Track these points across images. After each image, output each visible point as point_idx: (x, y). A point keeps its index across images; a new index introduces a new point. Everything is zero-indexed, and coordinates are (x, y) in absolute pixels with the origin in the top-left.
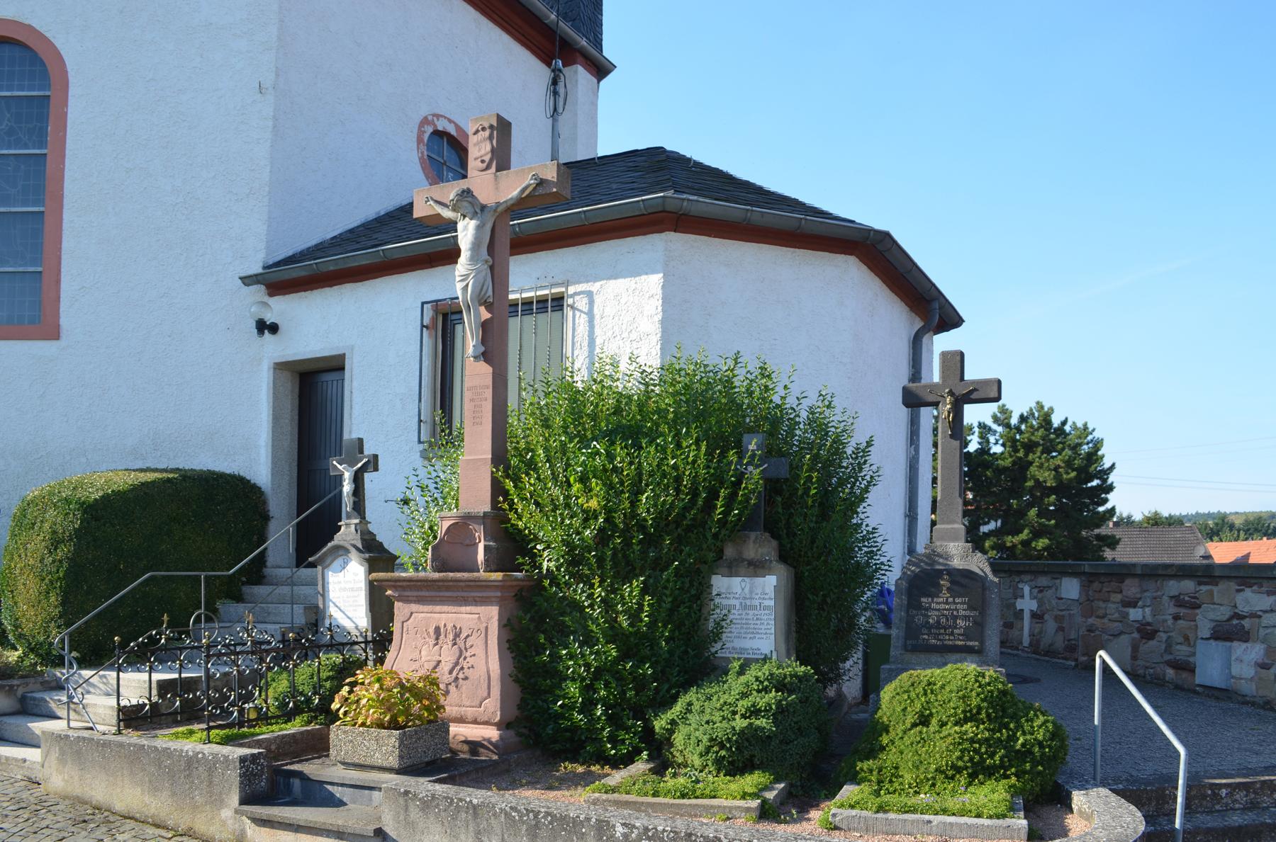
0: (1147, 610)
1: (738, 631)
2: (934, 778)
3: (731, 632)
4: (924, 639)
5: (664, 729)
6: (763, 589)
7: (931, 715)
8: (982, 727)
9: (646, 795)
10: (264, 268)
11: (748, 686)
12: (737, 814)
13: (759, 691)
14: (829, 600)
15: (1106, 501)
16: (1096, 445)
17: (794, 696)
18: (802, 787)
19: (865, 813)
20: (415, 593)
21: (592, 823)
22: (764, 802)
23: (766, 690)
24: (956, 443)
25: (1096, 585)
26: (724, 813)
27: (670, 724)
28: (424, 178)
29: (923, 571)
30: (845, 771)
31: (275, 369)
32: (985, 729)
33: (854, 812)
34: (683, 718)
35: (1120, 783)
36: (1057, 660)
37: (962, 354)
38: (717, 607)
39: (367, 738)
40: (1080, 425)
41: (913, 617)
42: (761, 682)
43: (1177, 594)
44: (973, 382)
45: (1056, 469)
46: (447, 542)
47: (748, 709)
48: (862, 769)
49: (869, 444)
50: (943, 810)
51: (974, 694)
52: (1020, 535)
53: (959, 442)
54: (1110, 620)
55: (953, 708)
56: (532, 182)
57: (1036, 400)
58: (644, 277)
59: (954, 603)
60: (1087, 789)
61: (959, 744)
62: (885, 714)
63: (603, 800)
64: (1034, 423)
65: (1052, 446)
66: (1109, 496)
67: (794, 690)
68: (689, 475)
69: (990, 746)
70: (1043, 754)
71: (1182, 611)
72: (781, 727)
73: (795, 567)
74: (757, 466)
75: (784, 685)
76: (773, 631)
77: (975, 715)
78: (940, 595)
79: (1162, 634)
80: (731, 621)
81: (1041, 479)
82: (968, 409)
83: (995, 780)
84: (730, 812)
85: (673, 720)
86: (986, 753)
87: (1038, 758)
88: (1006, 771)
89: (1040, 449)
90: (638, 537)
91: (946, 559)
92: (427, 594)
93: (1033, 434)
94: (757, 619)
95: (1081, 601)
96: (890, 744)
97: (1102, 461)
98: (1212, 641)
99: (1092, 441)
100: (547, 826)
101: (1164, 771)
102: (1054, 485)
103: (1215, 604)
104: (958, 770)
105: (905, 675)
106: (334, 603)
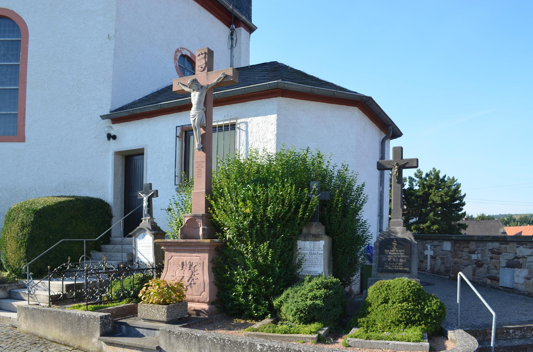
0: (479, 255)
1: (308, 264)
2: (390, 325)
3: (305, 264)
4: (386, 267)
5: (277, 305)
6: (319, 246)
7: (389, 299)
8: (410, 304)
9: (270, 332)
10: (110, 112)
11: (313, 287)
12: (308, 340)
13: (317, 289)
14: (346, 251)
15: (462, 209)
16: (458, 186)
17: (332, 291)
18: (335, 329)
19: (361, 340)
20: (174, 248)
21: (247, 344)
22: (319, 335)
23: (320, 288)
24: (400, 185)
25: (458, 245)
26: (302, 340)
27: (280, 303)
28: (177, 74)
29: (386, 239)
30: (353, 322)
31: (115, 154)
32: (412, 305)
33: (357, 340)
34: (285, 300)
35: (468, 327)
36: (442, 276)
37: (402, 148)
38: (299, 254)
39: (153, 309)
40: (451, 178)
41: (382, 258)
42: (318, 285)
43: (492, 248)
44: (406, 160)
45: (441, 196)
46: (187, 226)
47: (312, 296)
48: (360, 322)
49: (363, 186)
50: (394, 339)
51: (407, 290)
52: (426, 224)
53: (400, 185)
54: (463, 259)
55: (398, 296)
56: (222, 76)
57: (433, 167)
58: (269, 116)
59: (399, 252)
60: (454, 330)
61: (401, 311)
62: (370, 298)
63: (252, 334)
64: (432, 177)
65: (439, 186)
66: (463, 207)
67: (332, 288)
68: (288, 199)
69: (414, 312)
70: (436, 315)
71: (494, 255)
72: (326, 304)
73: (332, 237)
74: (316, 195)
75: (328, 287)
76: (323, 264)
77: (407, 299)
78: (393, 249)
79: (485, 265)
80: (305, 260)
81: (435, 200)
82: (404, 171)
83: (416, 326)
84: (305, 339)
85: (281, 301)
86: (412, 315)
87: (434, 317)
88: (420, 322)
89: (434, 188)
90: (266, 225)
91: (395, 234)
92: (178, 248)
93: (431, 181)
94: (316, 259)
95: (452, 251)
96: (372, 311)
97: (460, 193)
98: (506, 268)
99: (456, 184)
100: (228, 345)
101: (486, 322)
102: (440, 203)
103: (507, 252)
104: (400, 322)
105: (378, 282)
106: (139, 252)
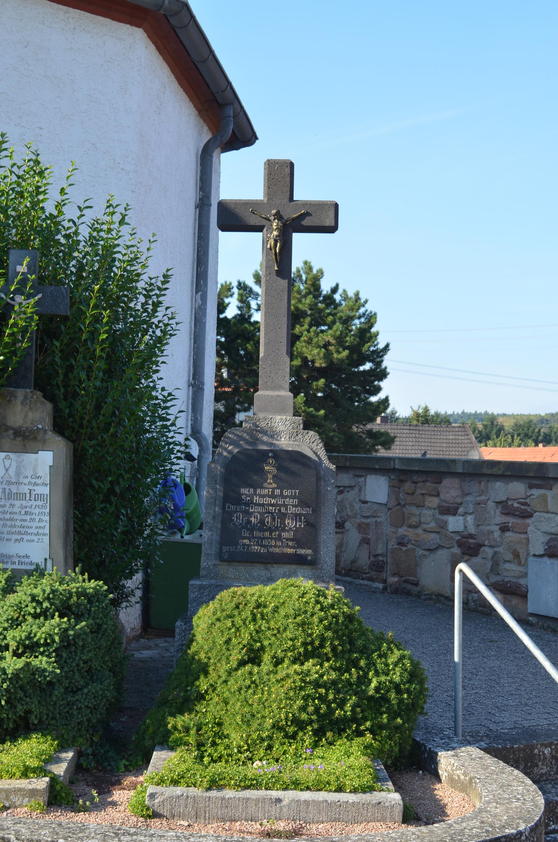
0: (470, 518)
2: (270, 738)
4: (244, 545)
7: (262, 648)
8: (326, 664)
11: (21, 609)
13: (36, 616)
14: (117, 489)
15: (378, 390)
16: (369, 320)
17: (84, 623)
18: (94, 755)
19: (193, 791)
22: (54, 780)
23: (45, 614)
24: (284, 283)
25: (408, 486)
29: (243, 452)
30: (151, 730)
32: (331, 667)
33: (178, 790)
35: (482, 741)
36: (361, 582)
37: (292, 165)
40: (351, 294)
41: (231, 514)
42: (40, 603)
43: (505, 499)
44: (306, 204)
45: (326, 345)
47: (20, 643)
48: (175, 728)
49: (166, 278)
50: (293, 783)
51: (315, 619)
53: (287, 280)
54: (425, 530)
55: (291, 639)
57: (304, 259)
59: (282, 496)
60: (454, 749)
61: (301, 688)
62: (202, 648)
64: (302, 287)
65: (321, 317)
66: (383, 384)
67: (82, 615)
69: (338, 691)
70: (401, 701)
71: (511, 521)
72: (66, 669)
73: (73, 442)
74: (29, 296)
75: (69, 608)
76: (47, 531)
77: (317, 648)
78: (265, 485)
79: (487, 549)
81: (310, 358)
82: (297, 238)
83: (346, 737)
84: (7, 798)
86: (334, 701)
87: (396, 707)
88: (359, 725)
89: (308, 320)
91: (272, 437)
95: (390, 506)
96: (210, 691)
97: (376, 340)
98: (545, 559)
99: (364, 314)
101: (526, 724)
102: (324, 365)
103: (548, 512)
104: (301, 725)
105: (225, 594)
